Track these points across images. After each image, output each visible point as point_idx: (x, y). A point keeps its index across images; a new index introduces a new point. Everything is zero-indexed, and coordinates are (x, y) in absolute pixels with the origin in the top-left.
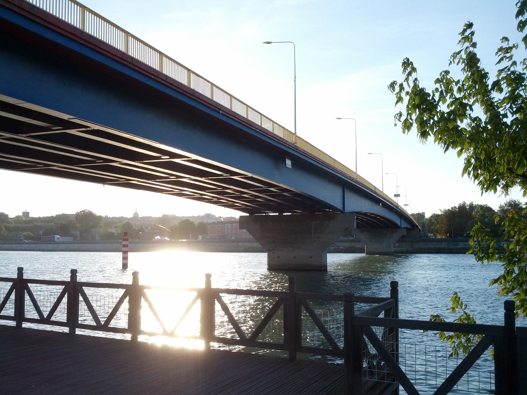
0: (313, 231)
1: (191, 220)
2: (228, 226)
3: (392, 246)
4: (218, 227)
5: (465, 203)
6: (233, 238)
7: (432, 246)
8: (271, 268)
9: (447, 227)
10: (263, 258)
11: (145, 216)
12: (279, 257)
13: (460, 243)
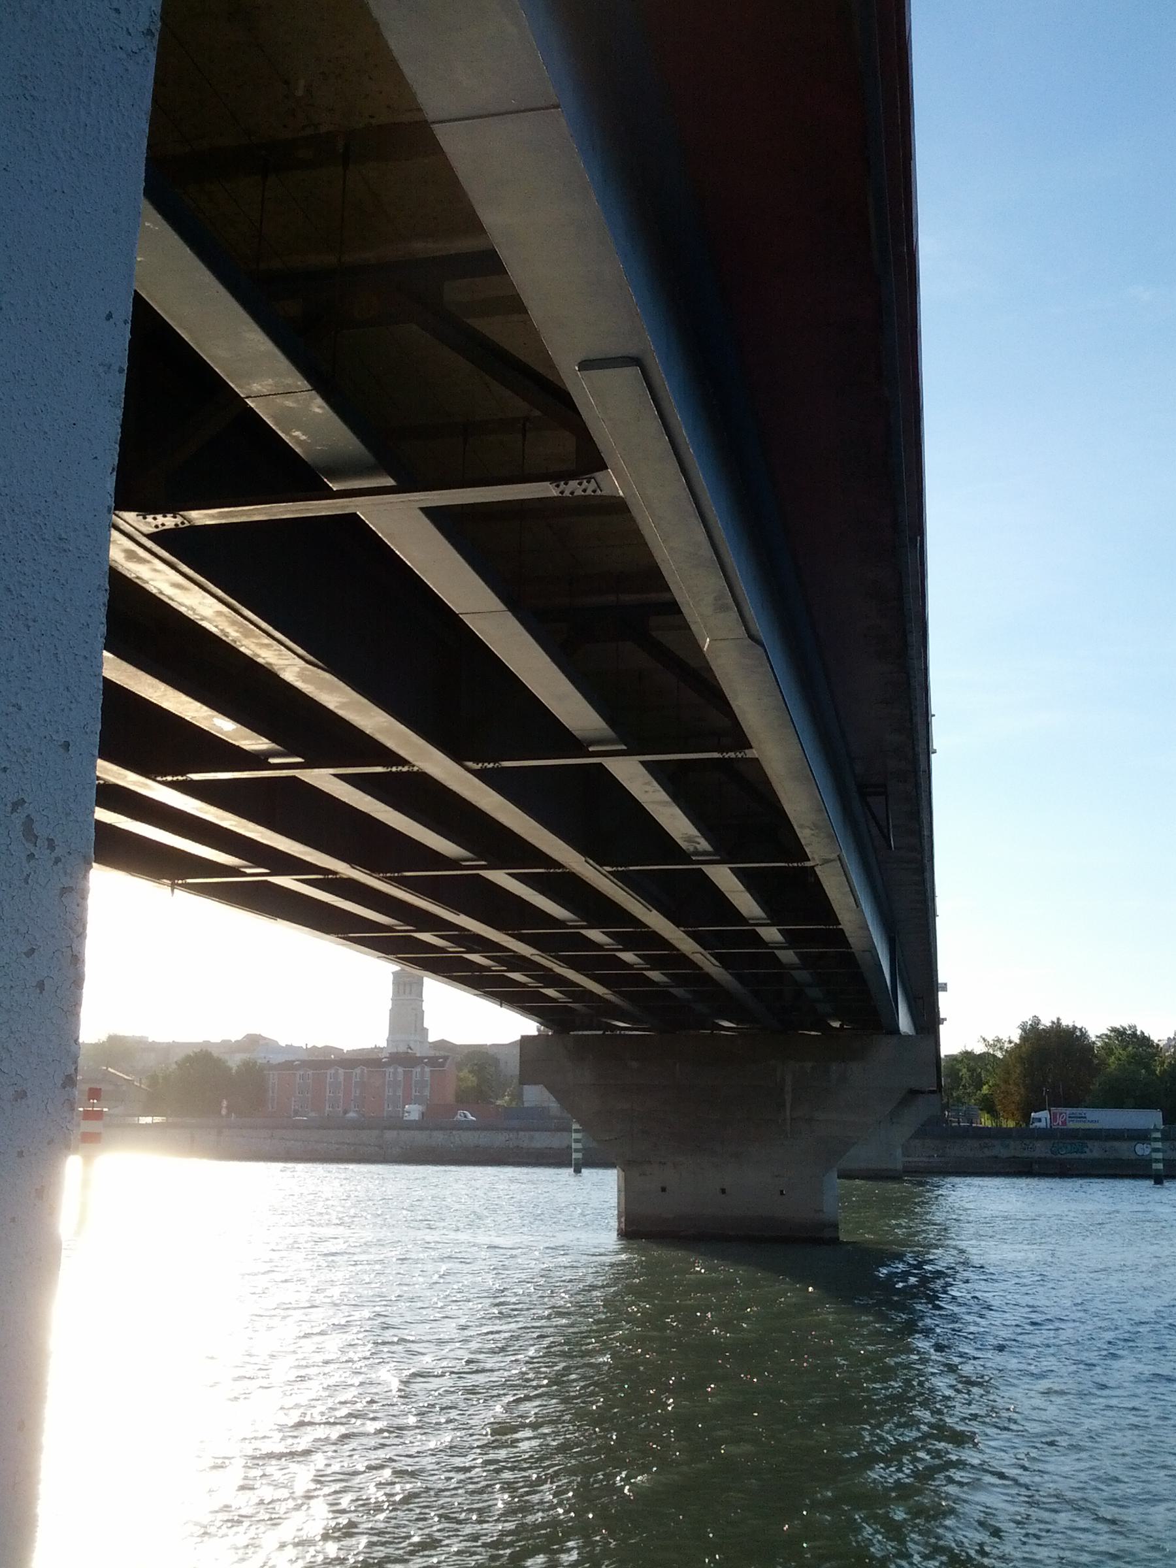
0: (788, 1098)
1: (215, 1055)
2: (395, 1073)
3: (899, 1151)
4: (302, 1077)
5: (1036, 1021)
6: (351, 1115)
7: (1004, 1153)
8: (634, 1229)
9: (1022, 1091)
10: (601, 1189)
11: (121, 1034)
12: (664, 1190)
13: (1090, 1143)
